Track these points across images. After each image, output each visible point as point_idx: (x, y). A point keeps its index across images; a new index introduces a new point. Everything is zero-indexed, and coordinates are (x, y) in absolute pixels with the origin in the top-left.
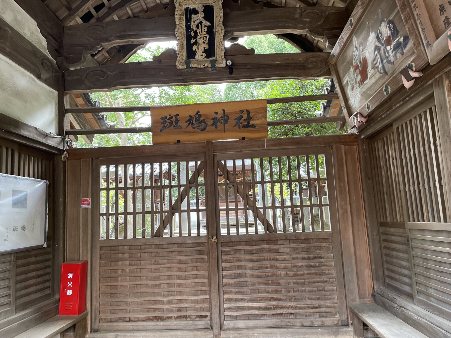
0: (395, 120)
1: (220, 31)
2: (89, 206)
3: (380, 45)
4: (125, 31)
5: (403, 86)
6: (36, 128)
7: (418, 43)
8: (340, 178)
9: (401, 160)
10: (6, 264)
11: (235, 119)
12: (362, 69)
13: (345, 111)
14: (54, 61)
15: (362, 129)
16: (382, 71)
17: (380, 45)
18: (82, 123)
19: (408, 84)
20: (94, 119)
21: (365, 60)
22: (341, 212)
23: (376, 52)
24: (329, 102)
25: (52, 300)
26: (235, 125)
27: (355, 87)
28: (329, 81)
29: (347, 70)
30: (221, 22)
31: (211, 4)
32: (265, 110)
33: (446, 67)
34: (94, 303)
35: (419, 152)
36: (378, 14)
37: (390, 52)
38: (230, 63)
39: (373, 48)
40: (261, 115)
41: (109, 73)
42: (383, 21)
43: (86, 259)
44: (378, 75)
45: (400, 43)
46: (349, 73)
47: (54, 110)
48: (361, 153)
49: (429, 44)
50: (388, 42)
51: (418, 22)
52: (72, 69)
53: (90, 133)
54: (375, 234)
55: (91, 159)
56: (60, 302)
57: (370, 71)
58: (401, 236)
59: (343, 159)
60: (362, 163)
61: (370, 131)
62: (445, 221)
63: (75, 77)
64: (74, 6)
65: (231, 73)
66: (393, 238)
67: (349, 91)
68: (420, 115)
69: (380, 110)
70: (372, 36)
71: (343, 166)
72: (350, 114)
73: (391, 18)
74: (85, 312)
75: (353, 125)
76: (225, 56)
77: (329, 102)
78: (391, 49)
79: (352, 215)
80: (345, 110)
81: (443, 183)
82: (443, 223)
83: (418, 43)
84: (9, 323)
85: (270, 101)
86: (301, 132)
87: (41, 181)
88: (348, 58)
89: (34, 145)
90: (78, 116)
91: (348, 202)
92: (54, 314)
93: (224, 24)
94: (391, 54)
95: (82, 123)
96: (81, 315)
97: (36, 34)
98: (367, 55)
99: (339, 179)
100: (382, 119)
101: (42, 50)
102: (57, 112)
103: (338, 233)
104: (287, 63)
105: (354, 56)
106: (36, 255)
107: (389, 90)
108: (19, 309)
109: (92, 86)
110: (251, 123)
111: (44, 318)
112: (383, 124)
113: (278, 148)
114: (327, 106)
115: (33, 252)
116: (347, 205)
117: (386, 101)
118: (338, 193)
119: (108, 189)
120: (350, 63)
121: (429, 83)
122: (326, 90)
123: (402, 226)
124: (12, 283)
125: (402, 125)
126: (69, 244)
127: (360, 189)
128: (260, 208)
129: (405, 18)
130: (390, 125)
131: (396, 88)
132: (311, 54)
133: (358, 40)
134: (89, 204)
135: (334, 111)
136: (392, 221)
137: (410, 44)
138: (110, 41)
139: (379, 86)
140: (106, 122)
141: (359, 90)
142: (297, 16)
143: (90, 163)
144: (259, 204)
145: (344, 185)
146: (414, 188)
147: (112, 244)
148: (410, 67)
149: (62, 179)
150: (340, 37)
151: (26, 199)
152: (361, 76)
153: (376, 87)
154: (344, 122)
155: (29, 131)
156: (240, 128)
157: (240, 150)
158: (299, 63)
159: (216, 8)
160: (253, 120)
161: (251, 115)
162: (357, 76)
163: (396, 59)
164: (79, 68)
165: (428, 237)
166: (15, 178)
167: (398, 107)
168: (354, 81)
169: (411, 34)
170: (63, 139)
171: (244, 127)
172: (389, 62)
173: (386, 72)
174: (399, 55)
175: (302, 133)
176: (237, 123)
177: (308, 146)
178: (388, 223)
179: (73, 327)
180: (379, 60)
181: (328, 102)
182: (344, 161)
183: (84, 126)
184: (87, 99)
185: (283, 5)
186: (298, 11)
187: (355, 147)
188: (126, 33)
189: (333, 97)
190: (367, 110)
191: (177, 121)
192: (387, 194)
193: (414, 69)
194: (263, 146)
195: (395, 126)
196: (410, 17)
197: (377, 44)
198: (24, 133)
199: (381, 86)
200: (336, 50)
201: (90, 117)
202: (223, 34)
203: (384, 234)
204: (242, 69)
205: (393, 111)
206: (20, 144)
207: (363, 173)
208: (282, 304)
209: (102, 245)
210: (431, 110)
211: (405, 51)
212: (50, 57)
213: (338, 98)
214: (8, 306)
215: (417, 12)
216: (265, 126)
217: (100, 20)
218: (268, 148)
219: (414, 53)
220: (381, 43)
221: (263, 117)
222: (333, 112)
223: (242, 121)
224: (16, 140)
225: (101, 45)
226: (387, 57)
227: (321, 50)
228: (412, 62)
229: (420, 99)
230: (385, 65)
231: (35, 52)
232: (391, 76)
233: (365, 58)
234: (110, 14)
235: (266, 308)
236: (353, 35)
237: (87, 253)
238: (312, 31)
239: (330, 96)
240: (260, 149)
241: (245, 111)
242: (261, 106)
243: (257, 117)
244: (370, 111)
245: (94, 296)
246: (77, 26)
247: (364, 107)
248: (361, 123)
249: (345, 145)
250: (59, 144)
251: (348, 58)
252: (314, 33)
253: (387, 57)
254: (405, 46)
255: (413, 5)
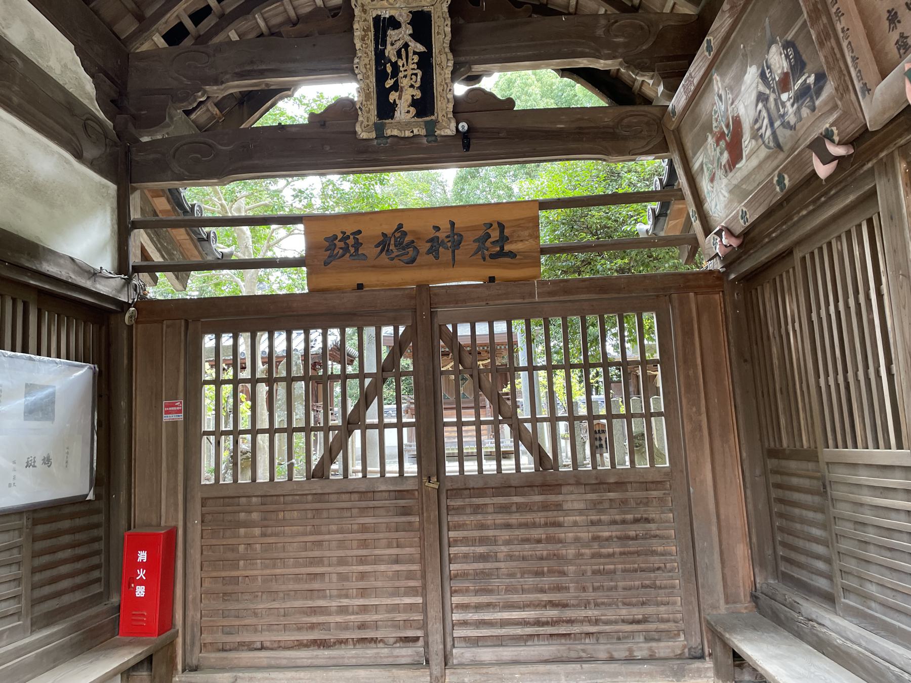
0: (799, 243)
1: (444, 64)
2: (180, 417)
3: (767, 92)
4: (252, 62)
5: (814, 174)
6: (72, 259)
7: (845, 87)
8: (687, 361)
9: (811, 323)
10: (11, 533)
11: (474, 241)
12: (732, 139)
13: (697, 225)
14: (110, 124)
15: (731, 260)
16: (772, 144)
17: (767, 92)
18: (165, 248)
19: (823, 171)
20: (189, 241)
21: (737, 122)
22: (688, 428)
23: (760, 106)
24: (665, 206)
25: (106, 607)
26: (476, 253)
27: (717, 177)
28: (665, 164)
29: (700, 142)
30: (447, 45)
31: (426, 9)
32: (535, 222)
33: (900, 136)
34: (190, 613)
35: (847, 307)
36: (764, 29)
37: (788, 104)
38: (464, 127)
39: (754, 96)
40: (526, 233)
41: (220, 147)
42: (773, 42)
43: (173, 524)
44: (763, 152)
45: (809, 87)
46: (706, 148)
47: (109, 222)
48: (729, 309)
49: (867, 90)
50: (784, 84)
51: (845, 44)
52: (145, 139)
53: (181, 270)
54: (758, 472)
55: (183, 322)
56: (121, 611)
57: (748, 144)
58: (810, 477)
59: (692, 321)
60: (731, 328)
61: (747, 265)
62: (900, 446)
63: (152, 156)
64: (149, 12)
65: (467, 147)
66: (795, 481)
67: (705, 185)
68: (848, 233)
69: (767, 223)
70: (752, 72)
71: (693, 334)
72: (707, 231)
73: (790, 37)
74: (172, 631)
75: (713, 252)
76: (455, 112)
77: (665, 206)
78: (789, 99)
79: (710, 434)
80: (698, 222)
81: (894, 371)
82: (894, 450)
83: (845, 87)
84: (19, 652)
85: (546, 205)
86: (609, 267)
87: (83, 367)
88: (704, 118)
89: (69, 293)
90: (157, 234)
91: (703, 409)
92: (109, 635)
93: (453, 48)
94: (790, 110)
95: (165, 248)
96: (164, 636)
97: (73, 68)
98: (742, 111)
99: (685, 362)
100: (772, 240)
101: (86, 102)
102: (116, 227)
103: (682, 471)
104: (580, 128)
105: (716, 112)
106: (72, 516)
107: (786, 181)
108: (38, 624)
109: (187, 173)
110: (507, 248)
111: (88, 642)
112: (775, 250)
113: (562, 298)
114: (660, 215)
115: (67, 510)
116: (700, 414)
117: (779, 205)
118: (683, 389)
119: (218, 383)
120: (708, 127)
121: (866, 168)
122: (658, 182)
123: (812, 456)
124: (24, 571)
125: (812, 253)
126: (140, 493)
127: (727, 382)
128: (526, 420)
129: (818, 36)
130: (788, 253)
131: (799, 177)
132: (628, 108)
133: (723, 81)
134: (179, 412)
135: (676, 225)
136: (792, 447)
137: (829, 89)
138: (222, 83)
139: (766, 173)
140: (214, 246)
141: (725, 181)
142: (600, 32)
143: (183, 329)
144: (524, 413)
145: (696, 374)
146: (836, 380)
147: (226, 494)
148: (828, 135)
149: (126, 361)
150: (687, 74)
151: (53, 402)
152: (730, 153)
153: (760, 177)
154: (695, 246)
155: (58, 265)
156: (484, 259)
157: (484, 303)
158: (604, 127)
159: (436, 17)
160: (511, 242)
161: (507, 232)
162: (721, 153)
163: (800, 119)
164: (159, 137)
165: (864, 478)
166: (31, 359)
167: (804, 217)
168: (715, 165)
169: (830, 68)
170: (128, 282)
171: (493, 256)
172: (786, 125)
173: (779, 146)
174: (805, 112)
175: (609, 269)
176: (479, 250)
177: (621, 295)
178: (784, 450)
179: (148, 661)
180: (766, 121)
181: (662, 207)
182: (696, 326)
183: (170, 254)
184: (176, 200)
185: (572, 10)
186: (603, 22)
187: (717, 296)
188: (255, 68)
189: (673, 196)
190: (742, 222)
191: (358, 245)
192: (782, 393)
193: (836, 138)
194: (532, 295)
195: (798, 255)
196: (829, 34)
197: (762, 88)
198: (48, 268)
199: (770, 174)
200: (679, 101)
201: (182, 237)
202: (451, 69)
203: (776, 472)
204: (489, 138)
205: (794, 224)
206: (40, 292)
207: (733, 349)
208: (569, 614)
209: (206, 496)
210: (870, 222)
211: (817, 103)
212: (101, 115)
213: (682, 198)
214: (16, 617)
215: (843, 24)
216: (536, 254)
217: (202, 40)
218: (541, 300)
219: (835, 107)
220: (769, 88)
221: (531, 236)
222: (672, 227)
223: (488, 244)
224: (32, 282)
225: (205, 92)
226: (783, 116)
227: (648, 101)
228: (831, 125)
229: (848, 201)
230: (778, 132)
231: (71, 104)
232: (790, 154)
233: (738, 116)
234: (222, 29)
235: (538, 623)
236: (713, 70)
237: (176, 510)
238: (630, 63)
239: (667, 194)
240: (526, 301)
241: (495, 225)
242: (527, 213)
243: (519, 236)
244: (747, 224)
245: (190, 597)
246: (155, 53)
247: (735, 217)
248: (729, 249)
249: (696, 294)
250: (120, 291)
251: (704, 118)
252: (635, 66)
253: (783, 116)
254: (818, 92)
255: (834, 10)
